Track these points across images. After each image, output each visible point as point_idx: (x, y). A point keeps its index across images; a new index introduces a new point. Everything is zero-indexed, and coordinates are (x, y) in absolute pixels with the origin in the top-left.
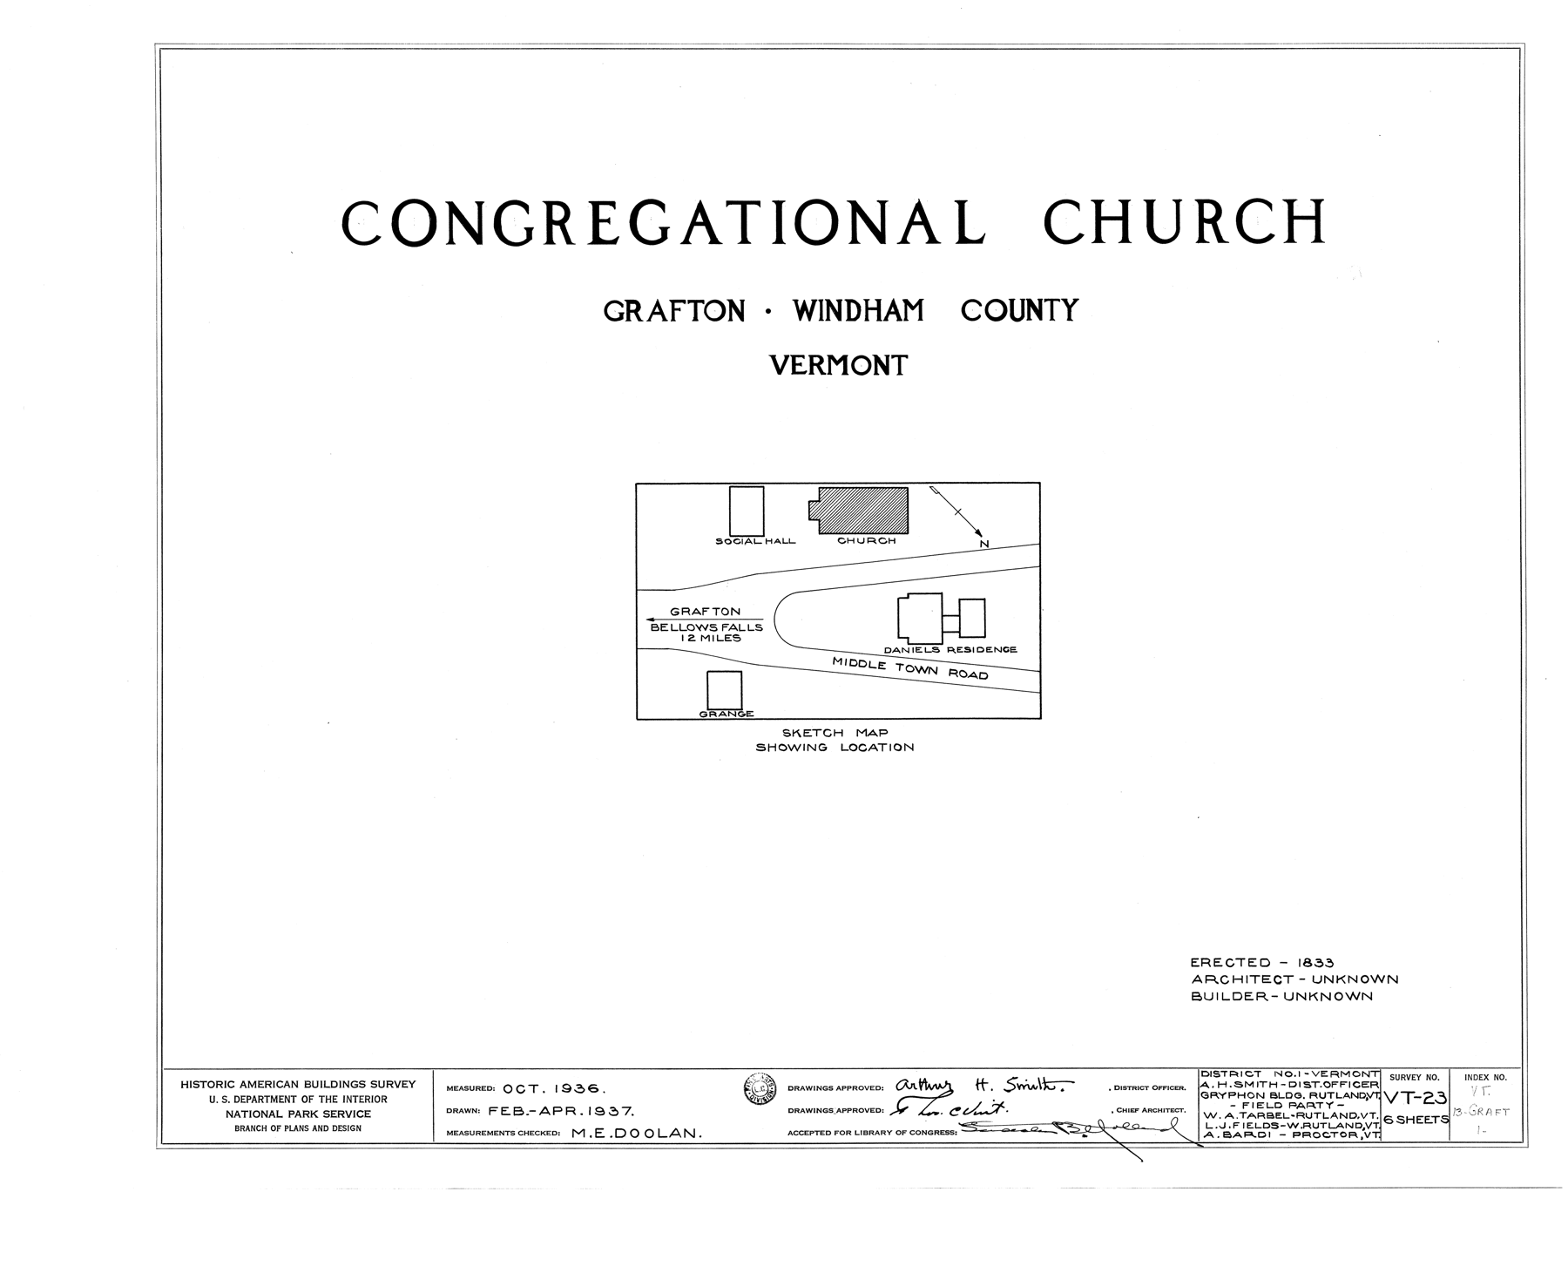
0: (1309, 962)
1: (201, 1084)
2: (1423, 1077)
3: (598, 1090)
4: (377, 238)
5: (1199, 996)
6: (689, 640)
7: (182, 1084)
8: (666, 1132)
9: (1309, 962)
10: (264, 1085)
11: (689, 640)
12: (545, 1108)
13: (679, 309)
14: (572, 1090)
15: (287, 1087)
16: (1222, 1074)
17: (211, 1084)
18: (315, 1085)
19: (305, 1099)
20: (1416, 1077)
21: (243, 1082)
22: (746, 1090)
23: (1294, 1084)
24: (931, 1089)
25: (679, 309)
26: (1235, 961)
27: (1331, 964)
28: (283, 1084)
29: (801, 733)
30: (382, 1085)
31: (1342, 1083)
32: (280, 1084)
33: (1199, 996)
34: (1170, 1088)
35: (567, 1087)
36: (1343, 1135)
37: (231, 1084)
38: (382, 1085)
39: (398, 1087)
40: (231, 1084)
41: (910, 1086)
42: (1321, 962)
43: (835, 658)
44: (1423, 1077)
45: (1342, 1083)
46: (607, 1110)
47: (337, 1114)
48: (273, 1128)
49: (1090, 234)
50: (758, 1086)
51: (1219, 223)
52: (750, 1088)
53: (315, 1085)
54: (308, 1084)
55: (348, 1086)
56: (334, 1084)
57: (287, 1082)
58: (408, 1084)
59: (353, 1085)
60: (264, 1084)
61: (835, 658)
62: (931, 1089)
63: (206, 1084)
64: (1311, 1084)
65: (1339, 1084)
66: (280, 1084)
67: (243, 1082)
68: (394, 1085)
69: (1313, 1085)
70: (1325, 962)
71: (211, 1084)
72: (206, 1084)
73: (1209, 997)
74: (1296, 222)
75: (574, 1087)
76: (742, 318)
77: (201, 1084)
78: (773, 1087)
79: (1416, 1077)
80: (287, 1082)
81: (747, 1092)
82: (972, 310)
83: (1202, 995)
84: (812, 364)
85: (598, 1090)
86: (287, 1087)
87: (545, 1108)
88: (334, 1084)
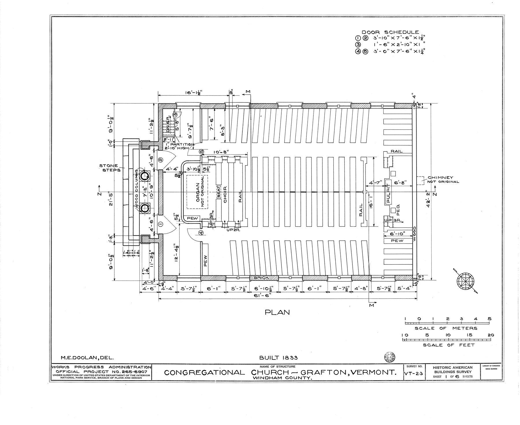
0: (288, 358)
1: (440, 368)
5: (263, 358)
7: (434, 368)
8: (88, 357)
9: (288, 358)
15: (469, 368)
17: (336, 372)
18: (438, 372)
22: (385, 357)
23: (137, 202)
27: (296, 358)
29: (66, 357)
31: (64, 371)
32: (466, 367)
33: (263, 358)
34: (451, 363)
37: (450, 368)
40: (450, 368)
42: (292, 357)
43: (62, 357)
45: (64, 371)
46: (290, 357)
50: (389, 356)
52: (386, 357)
53: (438, 372)
58: (469, 372)
59: (451, 372)
61: (62, 357)
64: (103, 165)
65: (62, 371)
66: (466, 367)
68: (464, 372)
69: (103, 166)
70: (294, 358)
71: (443, 368)
72: (441, 367)
73: (267, 358)
75: (419, 373)
77: (440, 368)
78: (394, 357)
81: (385, 358)
83: (264, 357)
86: (469, 368)
88: (444, 372)
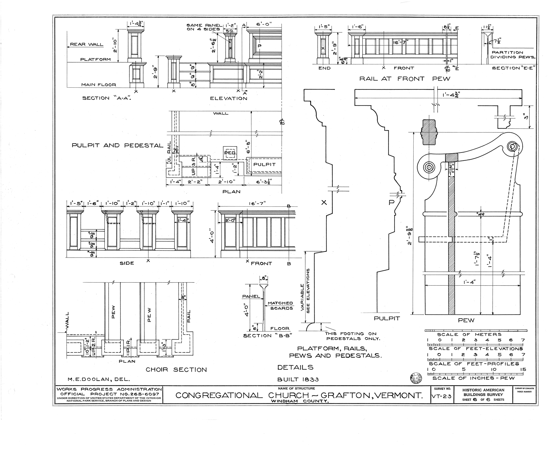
1: (470, 390)
2: (446, 389)
6: (131, 395)
7: (463, 390)
10: (492, 390)
11: (131, 395)
13: (212, 395)
15: (500, 391)
17: (473, 390)
19: (482, 400)
20: (443, 389)
21: (485, 389)
25: (212, 395)
26: (113, 394)
27: (450, 397)
28: (499, 390)
32: (498, 390)
34: (174, 386)
35: (91, 247)
36: (126, 394)
37: (480, 390)
40: (480, 390)
41: (114, 308)
44: (446, 389)
45: (69, 394)
48: (482, 400)
49: (302, 397)
50: (415, 377)
51: (294, 396)
53: (468, 395)
54: (488, 395)
55: (479, 395)
56: (474, 395)
57: (500, 389)
58: (500, 395)
60: (492, 390)
63: (471, 390)
65: (67, 394)
66: (498, 390)
67: (485, 389)
71: (473, 390)
77: (470, 390)
79: (443, 389)
80: (500, 389)
82: (179, 395)
86: (500, 391)
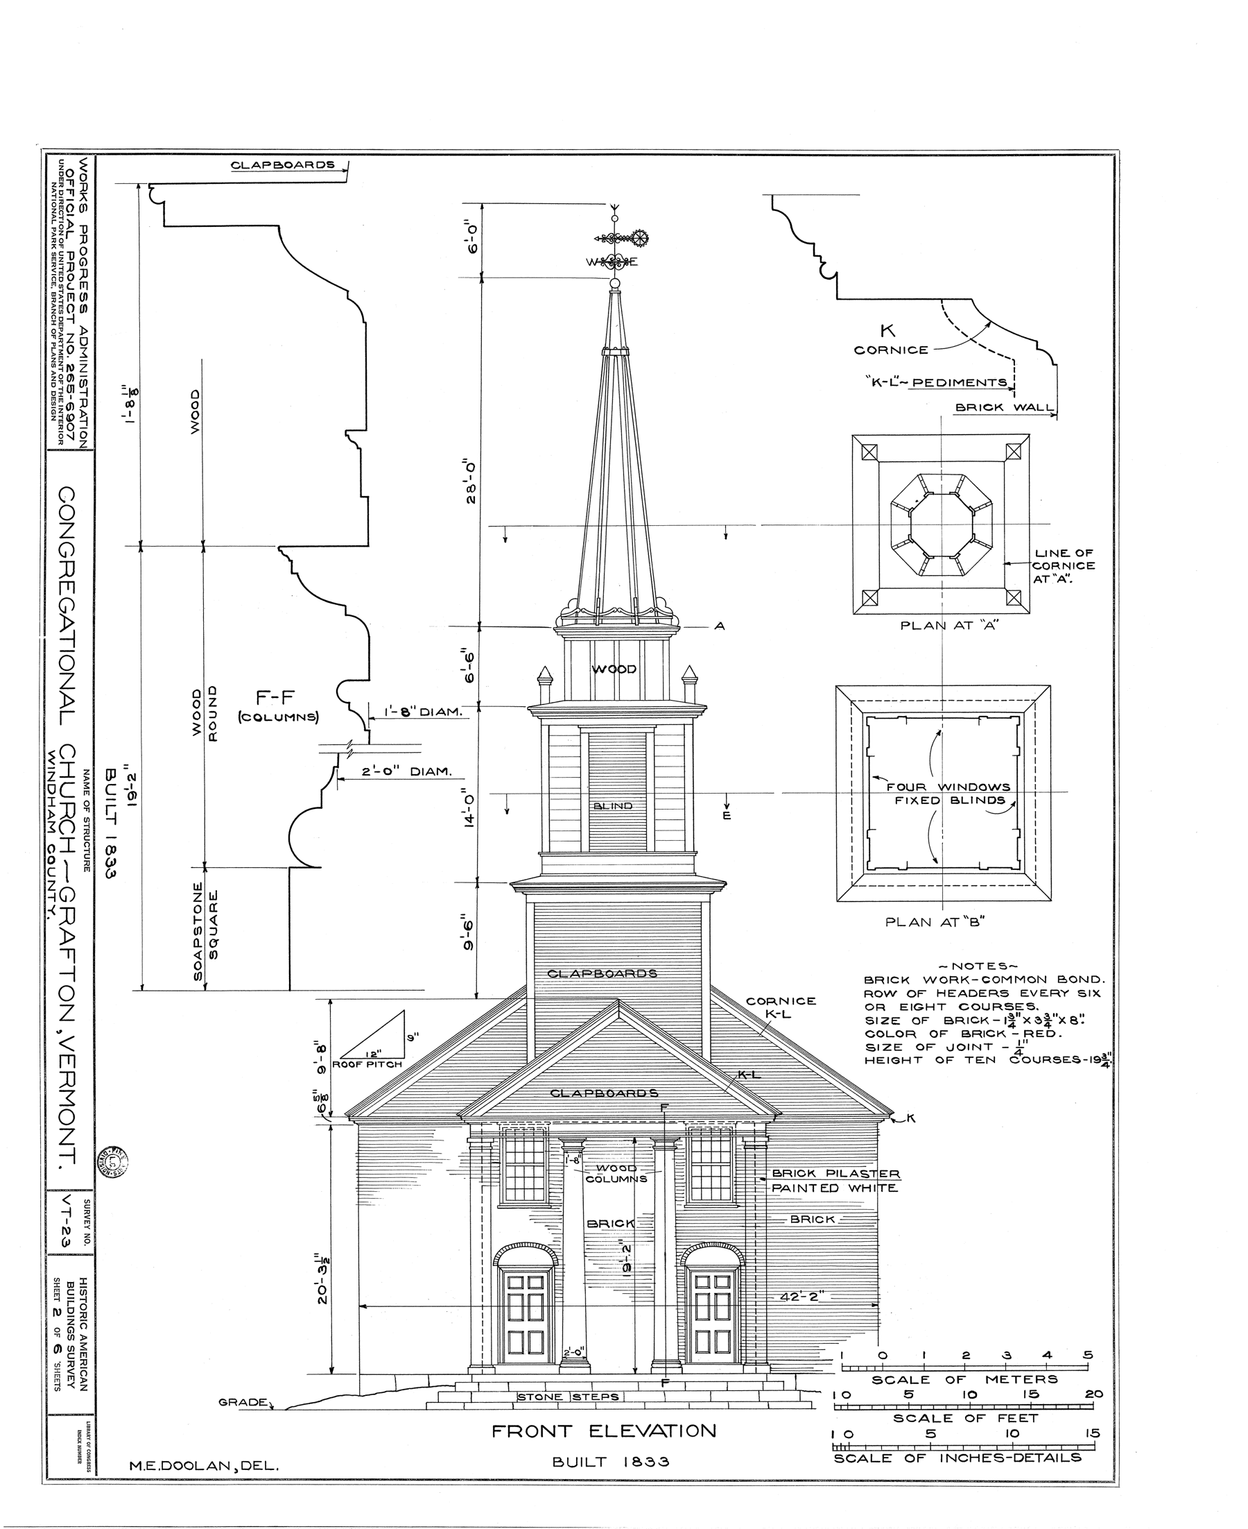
1: (84, 1297)
2: (87, 1231)
3: (1004, 802)
4: (65, 861)
7: (83, 1279)
12: (54, 815)
14: (657, 1464)
16: (84, 389)
17: (693, 1431)
18: (70, 1292)
20: (87, 1225)
21: (86, 1338)
22: (114, 1148)
24: (1020, 405)
28: (84, 1377)
30: (70, 1356)
32: (84, 1373)
34: (96, 1374)
38: (70, 1356)
39: (68, 1371)
40: (84, 1326)
44: (87, 1231)
47: (83, 1358)
50: (116, 1161)
52: (115, 1152)
53: (70, 1292)
56: (71, 1311)
58: (71, 1382)
62: (1020, 405)
66: (84, 1373)
67: (86, 1338)
71: (83, 1307)
72: (84, 1302)
74: (65, 910)
76: (82, 1390)
77: (84, 1297)
78: (113, 1176)
79: (87, 1225)
80: (86, 1380)
84: (84, 1360)
85: (56, 1353)
86: (81, 1380)
87: (54, 815)
